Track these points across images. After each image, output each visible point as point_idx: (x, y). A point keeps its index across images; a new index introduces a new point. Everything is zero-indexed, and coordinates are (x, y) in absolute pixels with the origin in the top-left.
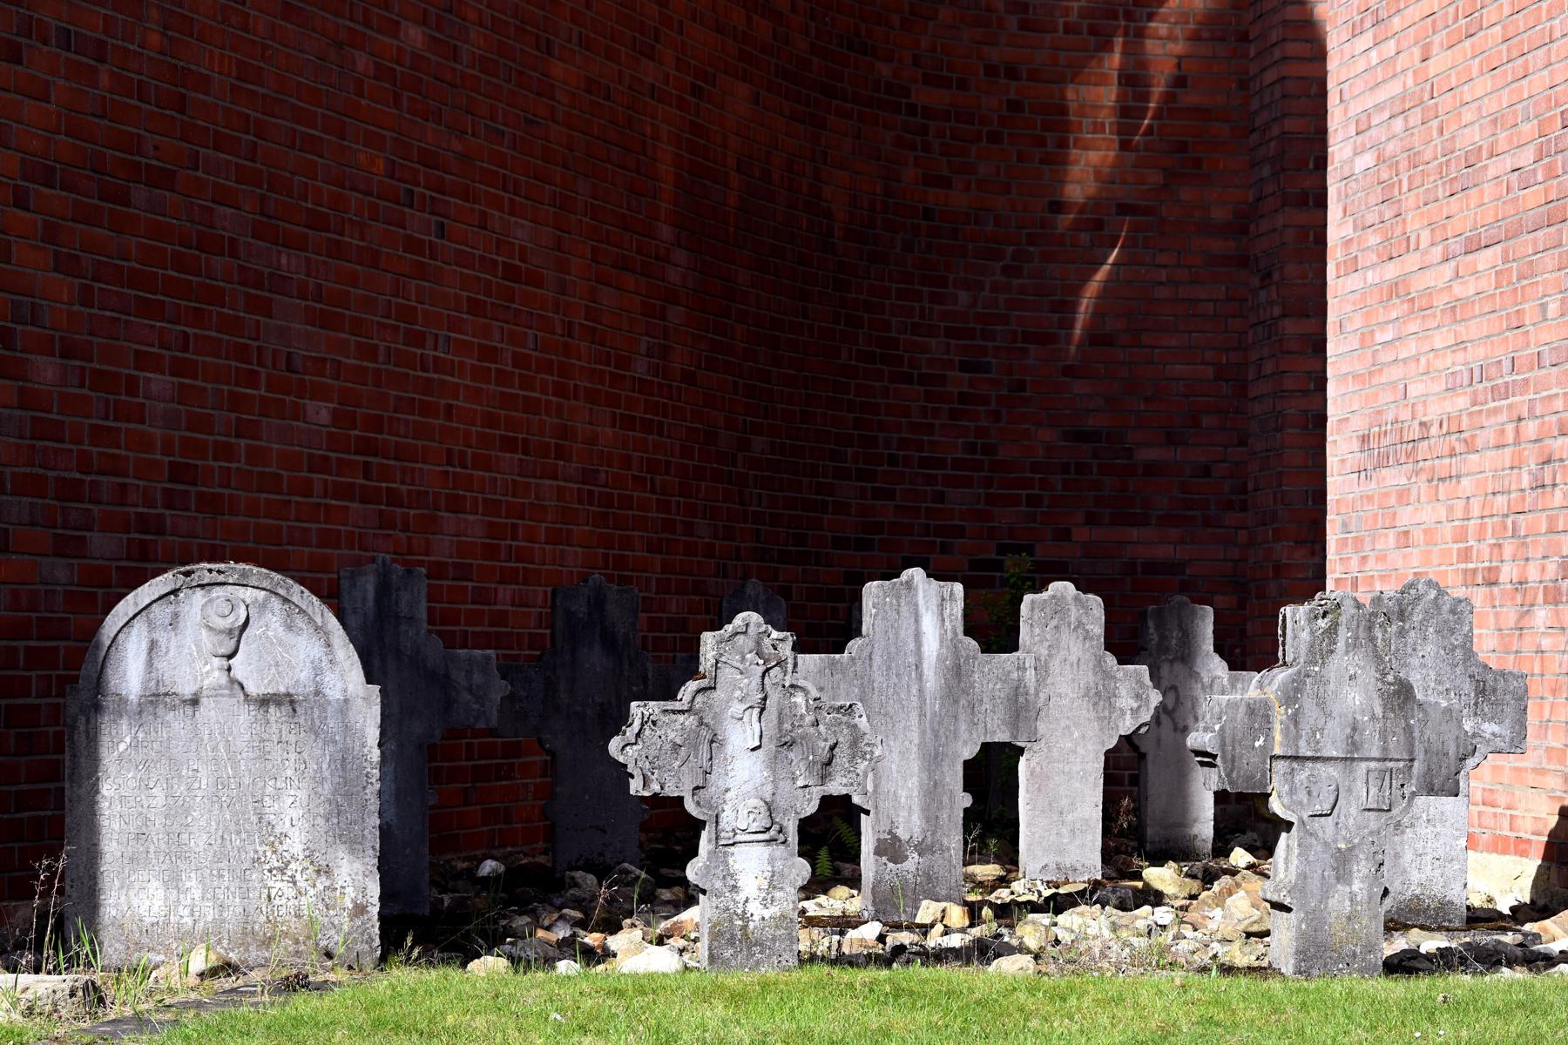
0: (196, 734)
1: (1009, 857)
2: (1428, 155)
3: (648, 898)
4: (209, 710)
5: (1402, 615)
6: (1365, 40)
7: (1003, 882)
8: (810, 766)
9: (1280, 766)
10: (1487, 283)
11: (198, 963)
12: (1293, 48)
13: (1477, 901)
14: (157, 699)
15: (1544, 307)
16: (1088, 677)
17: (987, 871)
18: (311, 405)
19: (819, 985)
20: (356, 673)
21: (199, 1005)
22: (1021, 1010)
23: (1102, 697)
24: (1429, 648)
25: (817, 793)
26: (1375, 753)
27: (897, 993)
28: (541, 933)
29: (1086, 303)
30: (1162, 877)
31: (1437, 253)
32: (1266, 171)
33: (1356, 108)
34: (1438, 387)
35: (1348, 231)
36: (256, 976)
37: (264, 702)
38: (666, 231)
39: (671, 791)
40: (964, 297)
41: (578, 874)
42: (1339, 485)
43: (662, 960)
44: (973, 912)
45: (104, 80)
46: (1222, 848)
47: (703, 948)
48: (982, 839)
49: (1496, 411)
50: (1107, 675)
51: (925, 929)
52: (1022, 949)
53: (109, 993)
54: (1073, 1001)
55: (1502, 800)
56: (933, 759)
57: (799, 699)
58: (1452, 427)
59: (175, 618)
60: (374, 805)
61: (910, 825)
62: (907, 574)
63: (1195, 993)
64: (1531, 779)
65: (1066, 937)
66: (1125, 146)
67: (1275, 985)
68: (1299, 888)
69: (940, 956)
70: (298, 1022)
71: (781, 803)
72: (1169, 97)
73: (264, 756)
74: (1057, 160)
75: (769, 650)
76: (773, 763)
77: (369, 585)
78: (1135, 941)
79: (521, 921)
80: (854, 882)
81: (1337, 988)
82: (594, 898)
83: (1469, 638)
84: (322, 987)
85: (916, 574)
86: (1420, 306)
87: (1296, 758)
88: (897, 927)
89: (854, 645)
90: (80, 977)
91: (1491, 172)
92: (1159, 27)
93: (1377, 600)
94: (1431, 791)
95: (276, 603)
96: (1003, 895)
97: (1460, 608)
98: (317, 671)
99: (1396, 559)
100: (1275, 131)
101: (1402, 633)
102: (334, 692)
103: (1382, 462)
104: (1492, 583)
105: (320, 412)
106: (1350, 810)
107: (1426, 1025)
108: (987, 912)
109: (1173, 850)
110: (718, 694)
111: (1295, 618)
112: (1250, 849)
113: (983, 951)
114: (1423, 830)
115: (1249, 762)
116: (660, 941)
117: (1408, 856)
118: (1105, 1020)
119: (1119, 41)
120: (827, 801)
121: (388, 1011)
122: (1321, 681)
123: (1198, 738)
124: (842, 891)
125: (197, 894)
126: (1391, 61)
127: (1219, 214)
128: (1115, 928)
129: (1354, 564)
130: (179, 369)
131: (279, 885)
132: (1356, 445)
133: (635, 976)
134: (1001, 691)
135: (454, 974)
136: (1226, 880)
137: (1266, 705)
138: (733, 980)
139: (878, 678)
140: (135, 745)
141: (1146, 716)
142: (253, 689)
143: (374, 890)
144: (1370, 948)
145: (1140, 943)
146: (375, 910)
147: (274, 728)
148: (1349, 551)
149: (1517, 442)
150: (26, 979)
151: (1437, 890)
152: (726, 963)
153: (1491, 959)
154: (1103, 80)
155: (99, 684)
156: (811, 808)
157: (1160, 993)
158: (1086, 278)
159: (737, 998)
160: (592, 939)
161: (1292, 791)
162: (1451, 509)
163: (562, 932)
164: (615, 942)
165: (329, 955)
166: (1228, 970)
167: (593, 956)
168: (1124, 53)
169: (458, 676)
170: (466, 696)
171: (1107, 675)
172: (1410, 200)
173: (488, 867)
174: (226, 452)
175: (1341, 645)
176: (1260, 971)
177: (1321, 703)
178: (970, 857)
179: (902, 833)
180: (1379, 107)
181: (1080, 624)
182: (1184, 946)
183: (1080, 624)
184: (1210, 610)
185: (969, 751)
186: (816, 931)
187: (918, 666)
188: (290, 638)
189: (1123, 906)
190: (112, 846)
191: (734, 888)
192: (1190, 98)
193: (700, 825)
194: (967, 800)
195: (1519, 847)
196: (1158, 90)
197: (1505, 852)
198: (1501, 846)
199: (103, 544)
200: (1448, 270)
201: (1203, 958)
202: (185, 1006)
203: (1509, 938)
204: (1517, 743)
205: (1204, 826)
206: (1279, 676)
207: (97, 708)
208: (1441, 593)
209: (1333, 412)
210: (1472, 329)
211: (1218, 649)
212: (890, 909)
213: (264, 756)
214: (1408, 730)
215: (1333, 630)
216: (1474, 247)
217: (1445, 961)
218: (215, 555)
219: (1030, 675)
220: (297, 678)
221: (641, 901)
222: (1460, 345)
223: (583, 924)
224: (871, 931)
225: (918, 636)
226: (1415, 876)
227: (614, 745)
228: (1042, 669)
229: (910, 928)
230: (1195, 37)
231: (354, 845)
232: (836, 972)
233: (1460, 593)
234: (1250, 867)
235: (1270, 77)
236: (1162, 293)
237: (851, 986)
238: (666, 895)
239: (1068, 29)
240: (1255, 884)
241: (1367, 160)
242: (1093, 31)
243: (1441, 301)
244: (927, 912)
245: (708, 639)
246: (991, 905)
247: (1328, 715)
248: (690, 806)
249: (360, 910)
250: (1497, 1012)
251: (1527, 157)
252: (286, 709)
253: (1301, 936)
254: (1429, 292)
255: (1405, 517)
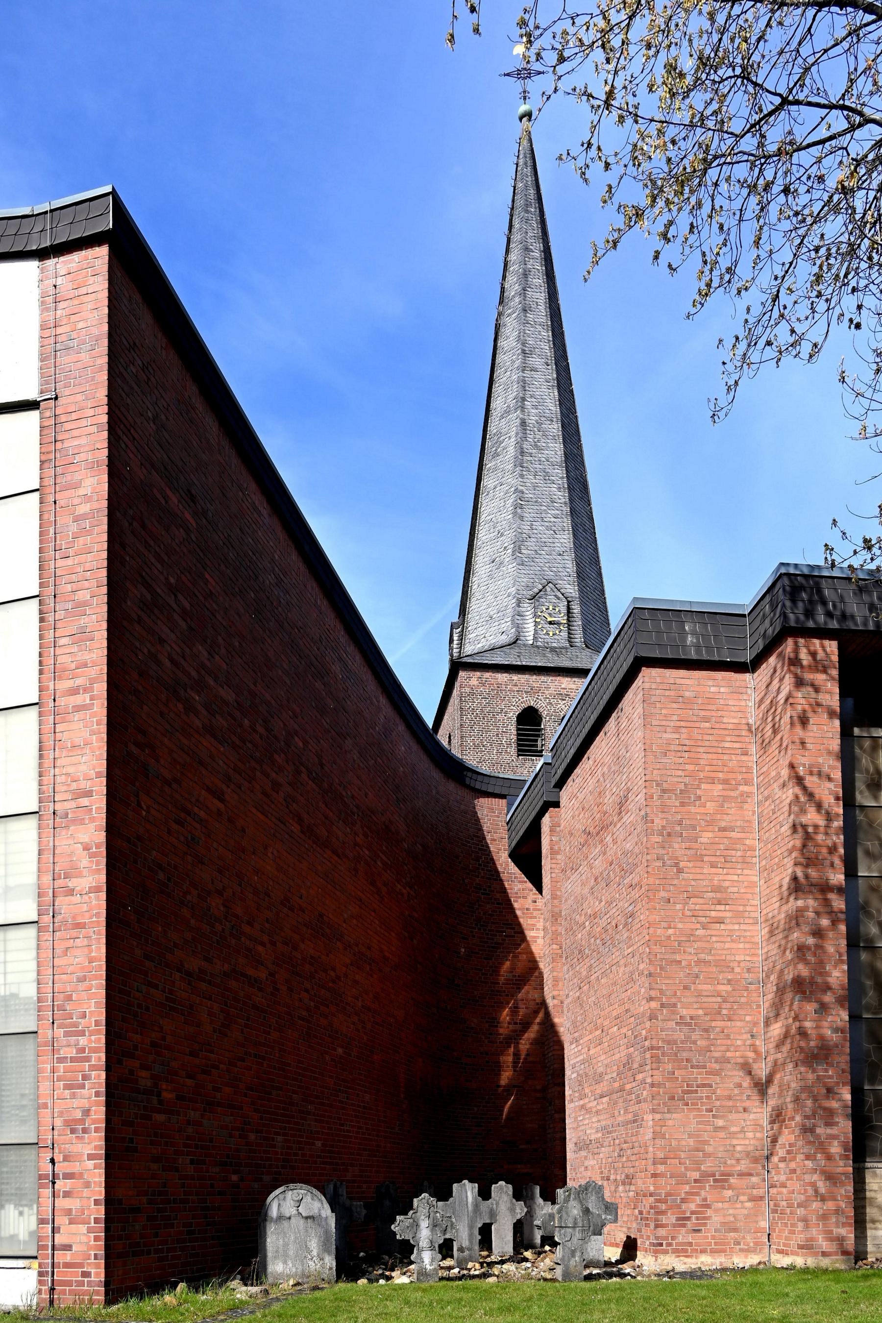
0: (290, 1226)
1: (489, 1249)
2: (590, 1074)
3: (401, 1262)
4: (293, 1220)
5: (586, 1189)
6: (574, 1046)
7: (489, 1256)
8: (441, 1232)
9: (557, 1229)
10: (605, 1106)
11: (291, 1282)
12: (556, 1047)
13: (606, 1259)
14: (280, 1218)
15: (620, 1112)
16: (509, 1205)
17: (485, 1253)
18: (317, 1142)
19: (444, 1286)
20: (329, 1211)
21: (292, 1294)
22: (494, 1292)
23: (512, 1210)
24: (593, 1198)
25: (443, 1238)
26: (581, 1225)
27: (464, 1288)
28: (375, 1272)
29: (506, 1110)
30: (528, 1254)
31: (593, 1098)
32: (550, 1078)
33: (572, 1062)
34: (594, 1131)
35: (571, 1092)
36: (305, 1286)
37: (307, 1218)
38: (402, 1096)
39: (407, 1238)
40: (476, 1109)
41: (384, 1256)
42: (570, 1155)
43: (405, 1280)
44: (482, 1264)
45: (265, 1065)
46: (542, 1246)
47: (415, 1276)
48: (482, 1248)
49: (608, 1137)
50: (513, 1204)
51: (470, 1270)
52: (494, 1275)
53: (270, 1292)
54: (507, 1290)
55: (612, 1234)
56: (471, 1227)
57: (438, 1215)
58: (597, 1141)
59: (284, 1199)
60: (334, 1243)
61: (466, 1243)
62: (463, 1182)
63: (537, 1287)
64: (619, 1229)
65: (504, 1271)
66: (515, 1071)
67: (557, 1284)
68: (563, 1259)
69: (474, 1277)
70: (317, 1299)
71: (434, 1240)
72: (525, 1059)
73: (307, 1231)
74: (499, 1075)
75: (430, 1203)
76: (432, 1231)
77: (331, 1187)
78: (522, 1272)
79: (370, 1269)
80: (452, 1257)
81: (572, 1285)
82: (388, 1262)
83: (603, 1195)
84: (322, 1289)
85: (466, 1182)
86: (589, 1111)
87: (561, 1227)
88: (463, 1269)
89: (451, 1199)
90: (263, 1287)
91: (606, 1078)
92: (523, 1042)
93: (580, 1186)
94: (595, 1234)
95: (309, 1194)
96: (489, 1260)
97: (601, 1188)
98: (320, 1210)
99: (584, 1174)
100: (552, 1068)
101: (586, 1194)
102: (324, 1215)
103: (580, 1150)
104: (608, 1180)
105: (319, 1144)
106: (575, 1240)
107: (595, 1295)
108: (485, 1265)
109: (530, 1246)
110: (418, 1214)
111: (560, 1192)
112: (549, 1246)
113: (485, 1276)
114: (593, 1243)
115: (549, 1228)
116: (405, 1274)
117: (589, 1249)
118: (515, 1295)
119: (513, 1045)
120: (445, 1239)
121: (339, 1296)
122: (567, 1207)
123: (536, 1223)
124: (449, 1259)
125: (291, 1265)
126: (579, 1051)
127: (538, 1087)
128: (517, 1268)
129: (574, 1174)
130: (284, 1135)
131: (311, 1263)
132: (573, 1145)
133: (398, 1284)
134: (488, 1210)
135: (354, 1284)
136: (544, 1254)
137: (553, 1214)
138: (423, 1285)
139: (457, 1208)
140: (275, 1229)
141: (523, 1214)
142: (304, 1215)
143: (334, 1264)
144: (580, 1274)
145: (523, 1272)
146: (334, 1269)
147: (309, 1224)
148: (572, 1172)
149: (614, 1145)
150: (250, 1288)
151: (596, 1257)
152: (421, 1280)
153: (610, 1275)
154: (509, 1055)
155: (266, 1214)
156: (441, 1242)
157: (529, 1287)
158: (506, 1103)
159: (424, 1290)
160: (387, 1273)
161: (560, 1235)
162: (598, 1161)
163: (380, 1272)
164: (393, 1274)
165: (323, 1280)
166: (545, 1280)
167: (389, 1278)
168: (514, 1048)
169: (354, 1209)
170: (356, 1214)
171: (513, 1204)
172: (586, 1085)
173: (362, 1254)
174: (296, 1154)
175: (571, 1199)
176: (553, 1280)
177: (567, 1213)
178: (482, 1250)
179: (464, 1246)
180: (578, 1062)
181: (506, 1192)
182: (534, 1273)
183: (506, 1192)
184: (538, 1187)
185: (480, 1225)
186: (443, 1271)
187: (467, 1204)
188: (313, 1202)
189: (519, 1263)
190: (270, 1254)
191: (423, 1262)
192: (531, 1059)
193: (415, 1246)
194: (479, 1237)
195: (617, 1245)
196: (523, 1056)
197: (613, 1246)
198: (612, 1245)
199: (266, 1178)
200: (595, 1102)
201: (539, 1276)
202: (288, 1294)
203: (615, 1269)
204: (616, 1220)
205: (538, 1241)
206: (557, 1207)
207: (265, 1220)
208: (596, 1184)
209: (568, 1137)
210: (601, 1117)
211: (541, 1196)
212: (461, 1265)
213: (307, 1231)
214: (589, 1219)
215: (569, 1195)
216: (602, 1097)
217: (599, 1276)
218: (294, 1181)
219: (495, 1206)
220: (315, 1211)
221: (399, 1263)
222: (599, 1121)
223: (385, 1269)
224: (456, 1270)
225: (467, 1197)
226: (591, 1254)
227: (393, 1227)
228: (497, 1204)
229: (466, 1269)
230: (531, 1044)
231: (329, 1253)
232: (448, 1282)
233: (600, 1184)
234: (550, 1250)
235: (550, 1054)
236: (525, 1107)
237: (452, 1287)
238: (405, 1261)
239: (500, 1042)
240: (552, 1256)
241: (575, 1075)
242: (506, 1043)
243: (594, 1110)
244: (470, 1265)
245: (415, 1200)
246: (486, 1263)
247: (569, 1216)
248: (412, 1242)
249: (331, 1269)
250: (612, 1291)
251: (615, 1075)
252: (312, 1219)
253: (563, 1271)
254: (591, 1108)
255: (586, 1163)
